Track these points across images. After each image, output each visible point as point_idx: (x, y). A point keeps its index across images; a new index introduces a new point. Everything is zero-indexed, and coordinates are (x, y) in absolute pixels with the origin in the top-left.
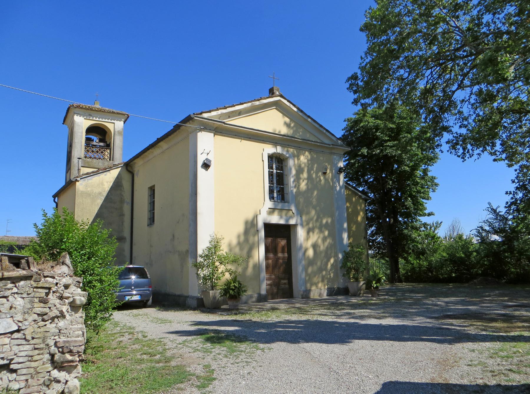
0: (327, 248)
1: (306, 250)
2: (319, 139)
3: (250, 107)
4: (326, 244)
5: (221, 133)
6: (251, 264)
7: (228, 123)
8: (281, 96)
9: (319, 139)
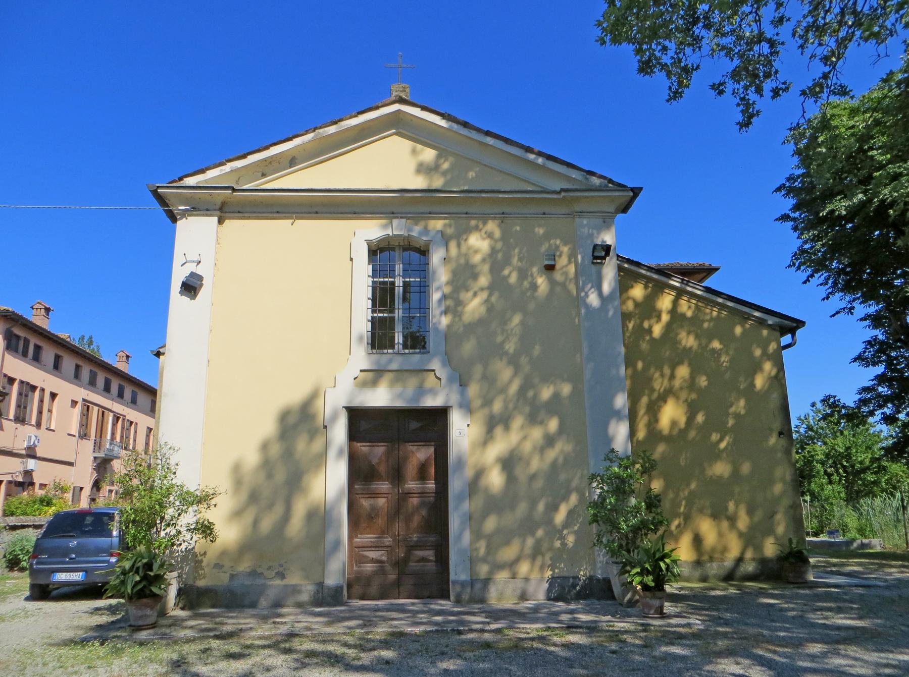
0: (554, 465)
2: (533, 184)
3: (310, 141)
4: (552, 454)
5: (239, 212)
6: (300, 509)
8: (402, 101)
9: (533, 184)
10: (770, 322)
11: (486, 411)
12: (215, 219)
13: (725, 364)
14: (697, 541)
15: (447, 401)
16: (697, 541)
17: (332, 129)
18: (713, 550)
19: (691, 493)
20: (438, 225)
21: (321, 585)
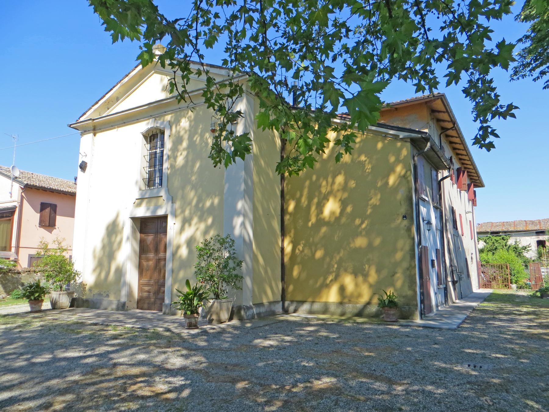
1: (178, 247)
7: (111, 113)
10: (401, 137)
11: (182, 215)
12: (92, 134)
13: (367, 171)
14: (342, 289)
15: (166, 211)
16: (342, 289)
17: (126, 79)
18: (352, 295)
19: (341, 259)
20: (168, 118)
21: (119, 301)
